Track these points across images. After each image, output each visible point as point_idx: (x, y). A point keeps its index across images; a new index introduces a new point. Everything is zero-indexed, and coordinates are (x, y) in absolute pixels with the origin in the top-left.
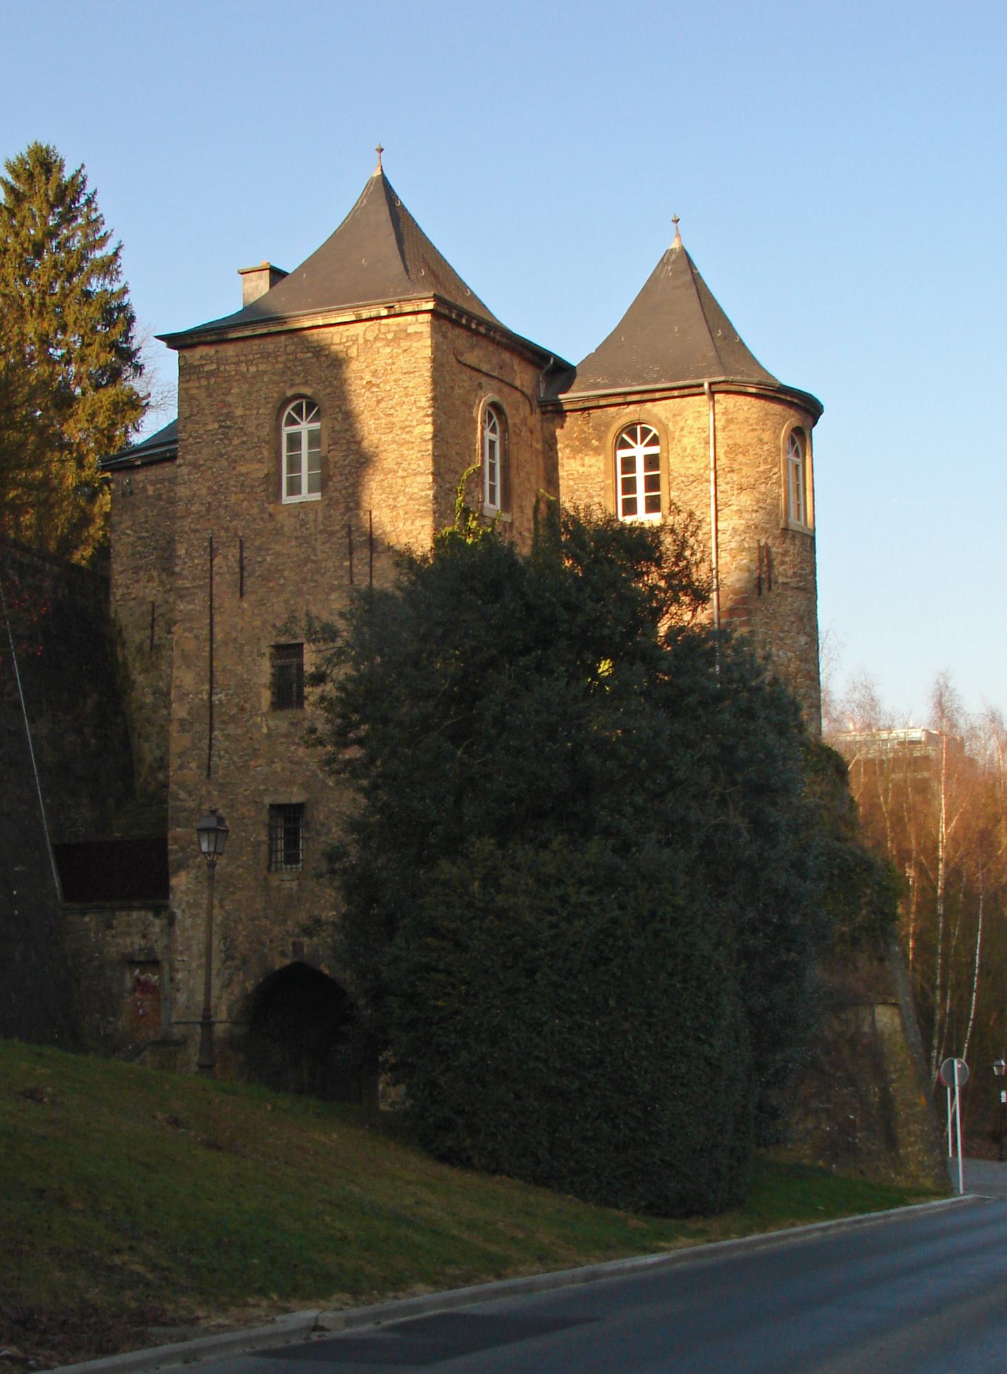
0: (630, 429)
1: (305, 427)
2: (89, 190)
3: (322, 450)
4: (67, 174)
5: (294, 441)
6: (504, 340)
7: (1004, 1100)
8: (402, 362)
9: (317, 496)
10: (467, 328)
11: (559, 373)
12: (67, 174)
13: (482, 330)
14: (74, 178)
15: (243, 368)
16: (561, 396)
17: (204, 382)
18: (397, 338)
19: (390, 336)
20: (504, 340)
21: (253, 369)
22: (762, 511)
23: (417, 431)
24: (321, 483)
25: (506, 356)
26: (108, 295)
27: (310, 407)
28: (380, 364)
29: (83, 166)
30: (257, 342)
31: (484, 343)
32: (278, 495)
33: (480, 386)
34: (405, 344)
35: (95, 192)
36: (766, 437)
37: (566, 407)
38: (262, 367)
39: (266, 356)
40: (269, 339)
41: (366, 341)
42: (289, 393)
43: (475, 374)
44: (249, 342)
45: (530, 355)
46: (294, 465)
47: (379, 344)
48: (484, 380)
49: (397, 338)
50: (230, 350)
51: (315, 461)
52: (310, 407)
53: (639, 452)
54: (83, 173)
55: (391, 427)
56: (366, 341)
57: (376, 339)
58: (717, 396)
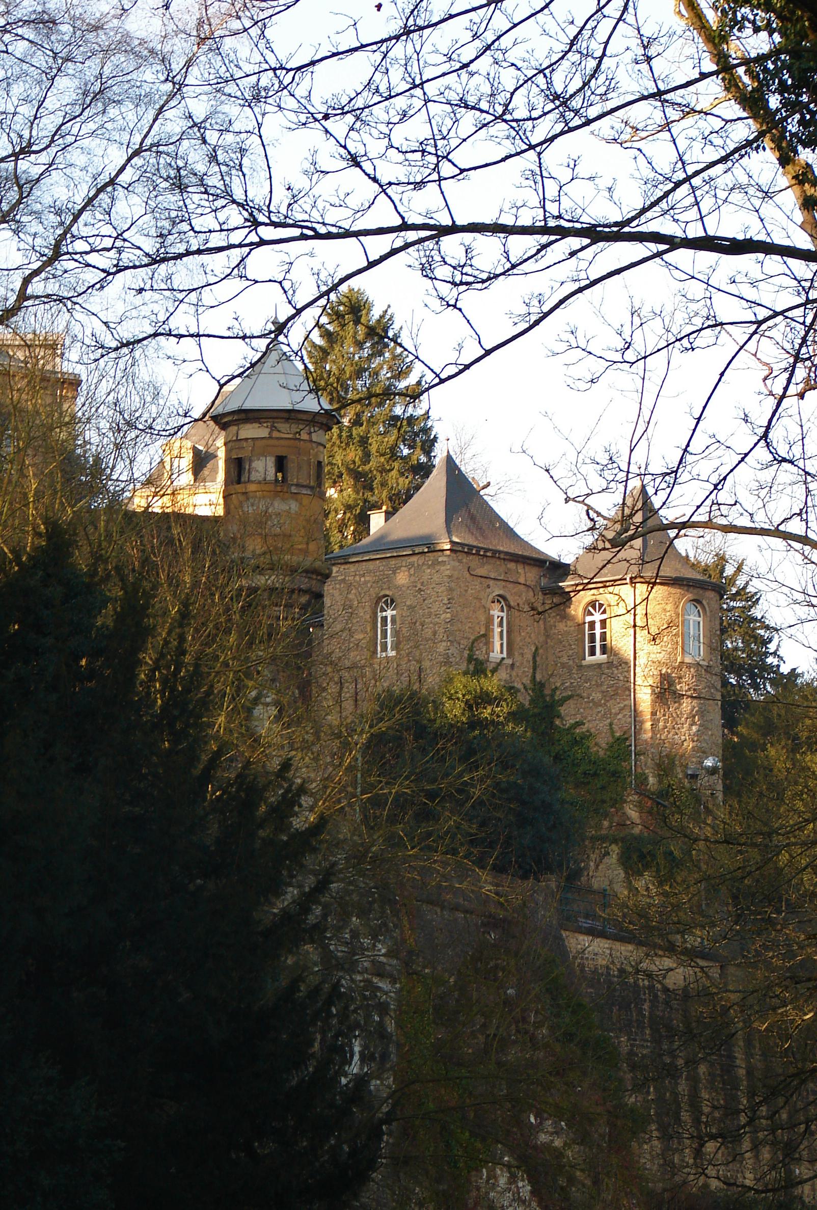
0: (593, 604)
1: (389, 613)
2: (396, 326)
3: (398, 626)
4: (376, 313)
5: (385, 619)
6: (508, 557)
7: (84, 660)
8: (436, 578)
9: (394, 653)
10: (478, 554)
11: (559, 569)
12: (376, 313)
13: (489, 554)
14: (382, 317)
15: (357, 578)
16: (560, 584)
17: (338, 586)
18: (433, 564)
19: (430, 563)
20: (508, 557)
21: (363, 579)
22: (664, 653)
23: (442, 617)
24: (397, 646)
25: (512, 565)
26: (411, 420)
27: (392, 601)
28: (425, 578)
29: (389, 306)
30: (364, 563)
31: (492, 561)
32: (375, 652)
33: (488, 586)
34: (437, 568)
35: (401, 328)
36: (668, 607)
37: (567, 590)
38: (367, 579)
39: (369, 572)
40: (371, 562)
41: (419, 565)
42: (382, 593)
43: (483, 579)
44: (361, 564)
45: (532, 562)
46: (384, 633)
47: (424, 567)
48: (491, 583)
49: (433, 564)
50: (352, 568)
51: (396, 633)
52: (392, 601)
53: (597, 617)
54: (389, 312)
55: (430, 614)
56: (419, 565)
57: (423, 564)
58: (638, 585)
